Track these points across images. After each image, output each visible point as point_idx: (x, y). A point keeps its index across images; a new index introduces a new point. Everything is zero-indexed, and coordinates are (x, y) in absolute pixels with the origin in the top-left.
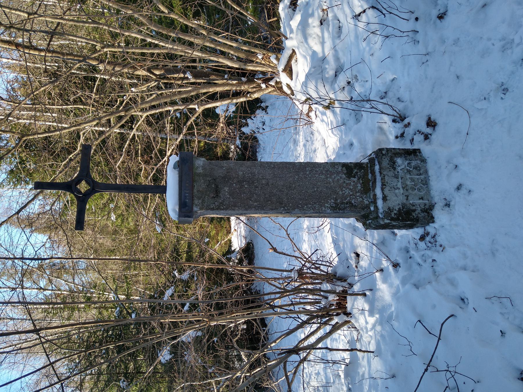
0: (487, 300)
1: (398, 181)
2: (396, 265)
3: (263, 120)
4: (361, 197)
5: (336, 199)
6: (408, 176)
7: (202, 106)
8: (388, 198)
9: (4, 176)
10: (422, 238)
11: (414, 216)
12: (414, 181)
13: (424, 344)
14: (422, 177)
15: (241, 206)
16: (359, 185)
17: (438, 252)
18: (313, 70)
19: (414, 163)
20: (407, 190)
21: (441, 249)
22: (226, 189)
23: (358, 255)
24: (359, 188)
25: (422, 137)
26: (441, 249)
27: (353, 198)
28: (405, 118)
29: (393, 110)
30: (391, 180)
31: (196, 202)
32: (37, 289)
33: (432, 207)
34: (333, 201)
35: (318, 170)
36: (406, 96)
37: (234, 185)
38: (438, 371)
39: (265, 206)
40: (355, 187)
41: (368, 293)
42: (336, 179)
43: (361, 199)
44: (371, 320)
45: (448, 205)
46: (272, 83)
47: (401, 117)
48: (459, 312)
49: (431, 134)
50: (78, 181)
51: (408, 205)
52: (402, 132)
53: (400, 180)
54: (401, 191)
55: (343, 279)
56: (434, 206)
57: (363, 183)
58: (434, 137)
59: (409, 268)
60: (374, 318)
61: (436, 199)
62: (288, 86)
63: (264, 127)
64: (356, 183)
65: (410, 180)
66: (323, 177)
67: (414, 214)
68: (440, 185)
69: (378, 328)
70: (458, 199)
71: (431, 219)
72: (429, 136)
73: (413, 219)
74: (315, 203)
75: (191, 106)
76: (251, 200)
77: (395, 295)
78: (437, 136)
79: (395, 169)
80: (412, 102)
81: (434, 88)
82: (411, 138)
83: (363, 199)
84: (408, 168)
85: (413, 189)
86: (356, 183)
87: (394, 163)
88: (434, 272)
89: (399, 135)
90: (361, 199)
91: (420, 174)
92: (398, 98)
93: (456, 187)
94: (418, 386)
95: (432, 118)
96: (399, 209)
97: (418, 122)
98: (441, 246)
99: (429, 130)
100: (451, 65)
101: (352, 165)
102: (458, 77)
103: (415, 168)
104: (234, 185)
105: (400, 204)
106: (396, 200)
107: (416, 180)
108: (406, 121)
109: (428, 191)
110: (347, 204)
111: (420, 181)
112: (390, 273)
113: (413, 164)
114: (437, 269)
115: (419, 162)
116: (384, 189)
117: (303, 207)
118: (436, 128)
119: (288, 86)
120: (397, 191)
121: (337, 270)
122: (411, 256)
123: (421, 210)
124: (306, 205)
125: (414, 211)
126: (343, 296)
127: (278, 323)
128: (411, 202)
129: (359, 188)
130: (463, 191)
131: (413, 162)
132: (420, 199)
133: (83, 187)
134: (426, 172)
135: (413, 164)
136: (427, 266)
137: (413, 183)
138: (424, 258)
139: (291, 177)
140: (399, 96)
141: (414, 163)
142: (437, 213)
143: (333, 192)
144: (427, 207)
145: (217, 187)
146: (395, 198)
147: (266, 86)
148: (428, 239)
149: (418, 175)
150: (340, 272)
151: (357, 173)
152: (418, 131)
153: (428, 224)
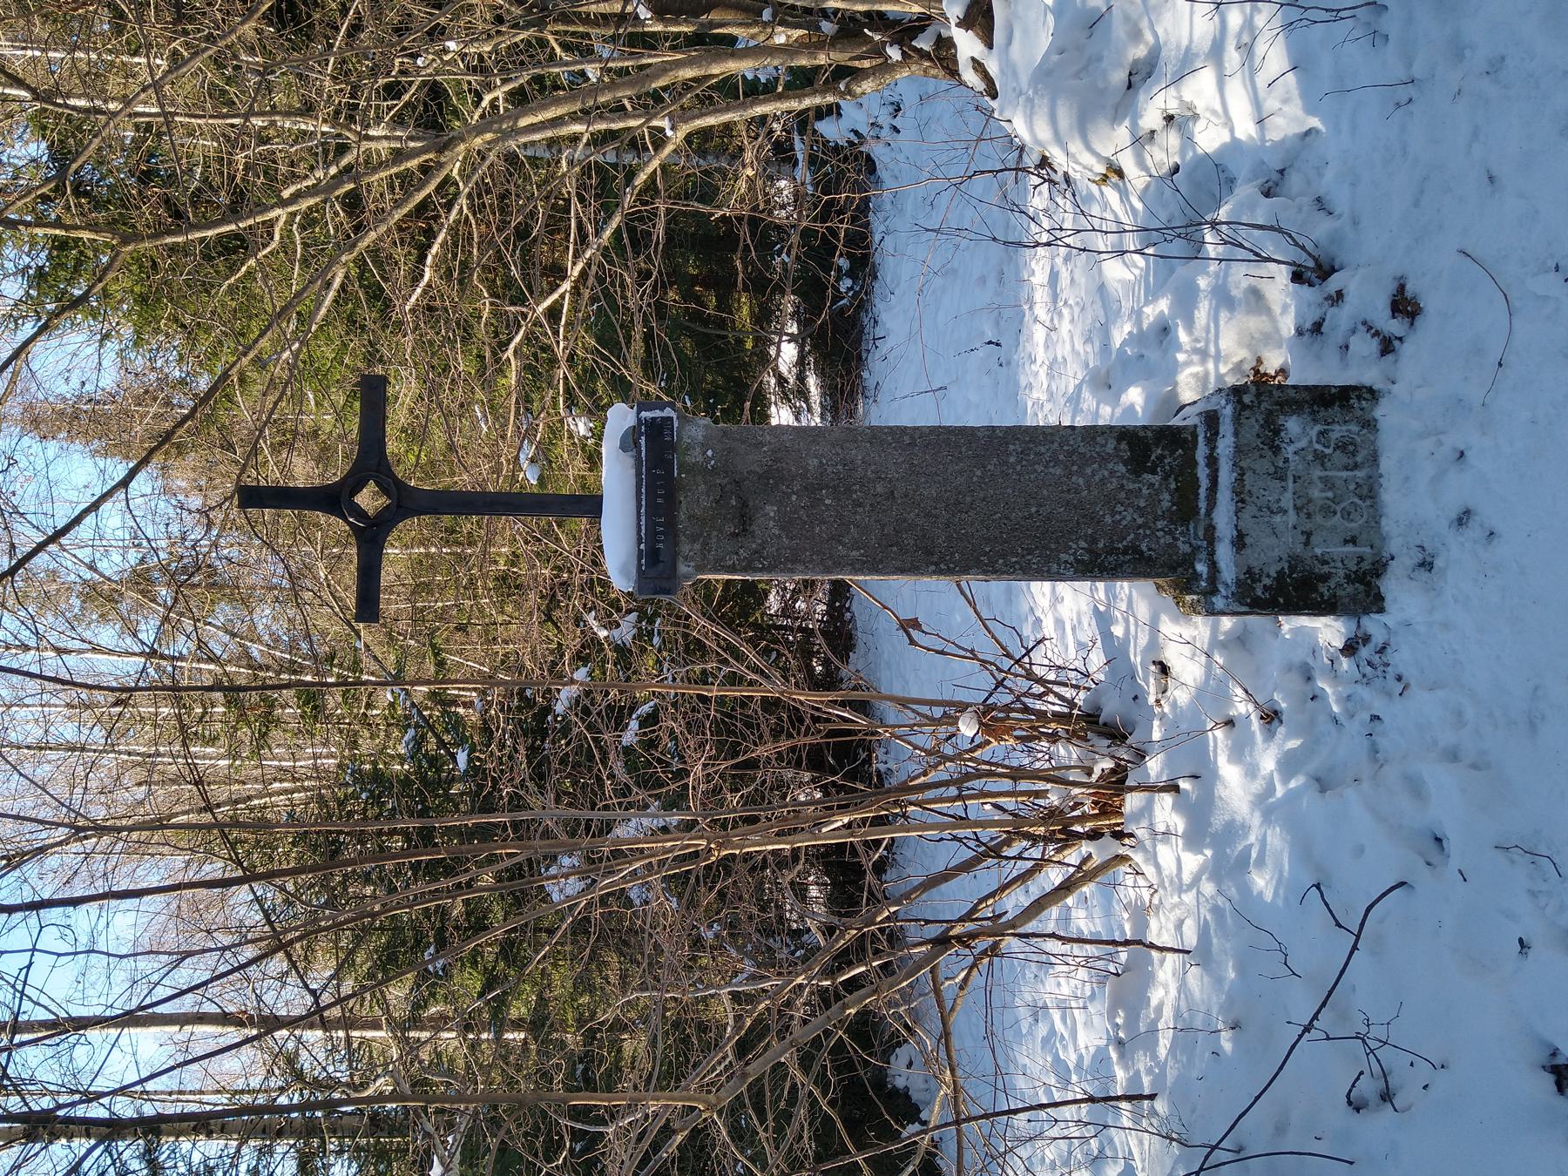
0: (1499, 853)
1: (1285, 489)
2: (1271, 717)
3: (897, 98)
4: (1170, 533)
5: (1093, 540)
6: (1317, 472)
7: (685, 122)
8: (1248, 540)
9: (14, 288)
10: (1350, 649)
11: (1322, 595)
12: (1332, 487)
13: (1318, 947)
14: (1360, 474)
15: (811, 561)
16: (1166, 496)
17: (1389, 695)
18: (1056, 57)
19: (1338, 431)
20: (1309, 516)
21: (1400, 687)
22: (771, 510)
23: (1164, 669)
24: (1166, 504)
25: (1374, 345)
26: (1399, 687)
27: (1146, 536)
28: (1333, 270)
29: (1296, 244)
30: (1262, 484)
31: (685, 548)
32: (141, 654)
33: (1380, 568)
34: (1083, 544)
35: (1043, 450)
36: (1341, 200)
37: (794, 498)
38: (1328, 1038)
39: (881, 561)
40: (1154, 500)
41: (1184, 785)
42: (1097, 478)
43: (1169, 539)
44: (1192, 862)
45: (1426, 565)
46: (924, 43)
47: (1319, 265)
48: (1421, 876)
49: (1400, 339)
50: (353, 482)
51: (1309, 562)
52: (1316, 318)
53: (1291, 484)
54: (1292, 517)
55: (1116, 735)
56: (1385, 565)
57: (1177, 489)
58: (1406, 349)
59: (1307, 729)
60: (1200, 858)
61: (1394, 546)
62: (978, 66)
63: (898, 122)
64: (1155, 489)
65: (1321, 486)
66: (1058, 471)
67: (1323, 588)
68: (1410, 502)
69: (1208, 888)
70: (1457, 552)
71: (1376, 603)
72: (1396, 343)
73: (1320, 604)
74: (1030, 551)
75: (655, 123)
76: (840, 542)
77: (1263, 801)
78: (1417, 348)
79: (1276, 450)
80: (1355, 222)
81: (1422, 192)
82: (1341, 341)
83: (1175, 539)
84: (1319, 447)
85: (1328, 511)
86: (1155, 489)
87: (1277, 432)
88: (1374, 750)
89: (1308, 325)
90: (1169, 539)
91: (1356, 466)
92: (1319, 200)
93: (1454, 516)
94: (1281, 1068)
95: (1410, 289)
96: (1281, 573)
97: (1365, 294)
98: (1399, 679)
99: (1394, 327)
100: (1475, 134)
101: (1150, 434)
102: (1491, 178)
103: (1342, 446)
104: (794, 498)
105: (1285, 557)
106: (1273, 549)
107: (1339, 483)
108: (1334, 283)
109: (1376, 518)
110: (1125, 553)
111: (1352, 487)
112: (1253, 733)
113: (1334, 436)
114: (1383, 742)
115: (1354, 428)
116: (1246, 501)
117: (992, 563)
118: (1419, 320)
119: (978, 66)
120: (1278, 519)
121: (1103, 700)
122: (1318, 692)
123: (1347, 577)
124: (1003, 556)
125: (1325, 578)
126: (1117, 782)
127: (925, 848)
128: (1318, 551)
129: (1166, 504)
130: (1474, 532)
131: (1336, 427)
132: (1346, 542)
133: (368, 499)
134: (1374, 459)
135: (1334, 436)
136: (1356, 727)
137: (1330, 494)
138: (1349, 705)
139: (961, 472)
140: (1321, 193)
141: (1338, 431)
142: (1393, 586)
143: (1084, 516)
144: (1366, 566)
145: (745, 504)
146: (1272, 540)
147: (904, 54)
148: (1365, 652)
149: (1346, 468)
150: (1112, 709)
151: (1161, 458)
152: (1364, 323)
153: (1367, 611)
